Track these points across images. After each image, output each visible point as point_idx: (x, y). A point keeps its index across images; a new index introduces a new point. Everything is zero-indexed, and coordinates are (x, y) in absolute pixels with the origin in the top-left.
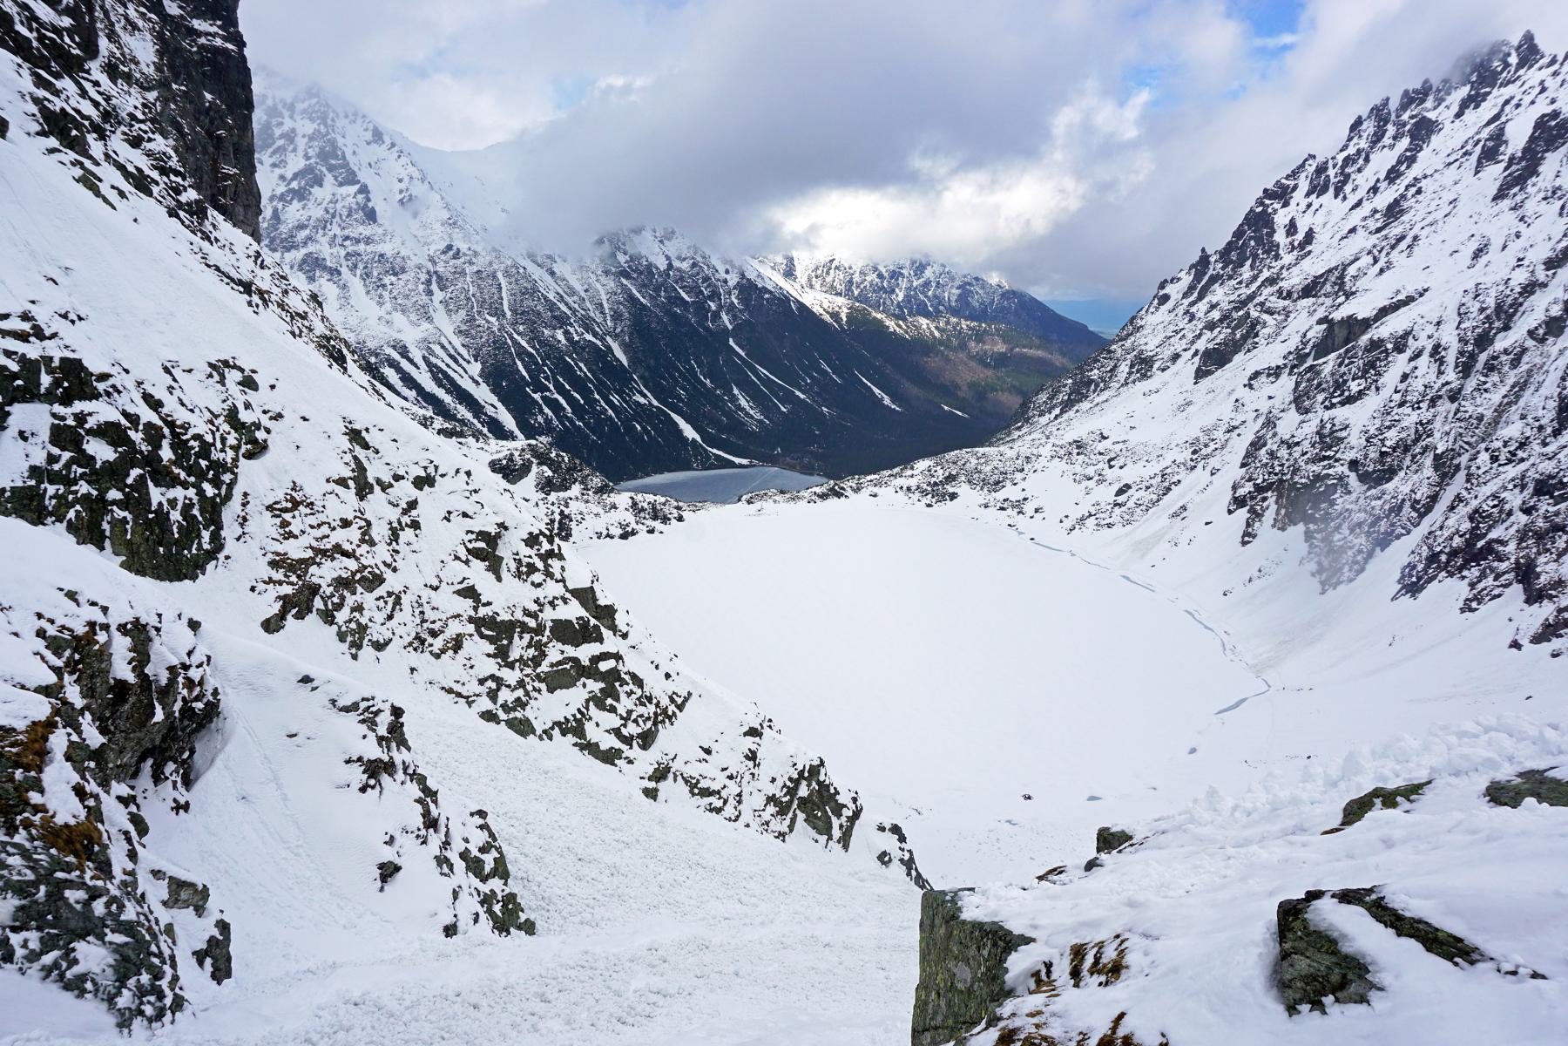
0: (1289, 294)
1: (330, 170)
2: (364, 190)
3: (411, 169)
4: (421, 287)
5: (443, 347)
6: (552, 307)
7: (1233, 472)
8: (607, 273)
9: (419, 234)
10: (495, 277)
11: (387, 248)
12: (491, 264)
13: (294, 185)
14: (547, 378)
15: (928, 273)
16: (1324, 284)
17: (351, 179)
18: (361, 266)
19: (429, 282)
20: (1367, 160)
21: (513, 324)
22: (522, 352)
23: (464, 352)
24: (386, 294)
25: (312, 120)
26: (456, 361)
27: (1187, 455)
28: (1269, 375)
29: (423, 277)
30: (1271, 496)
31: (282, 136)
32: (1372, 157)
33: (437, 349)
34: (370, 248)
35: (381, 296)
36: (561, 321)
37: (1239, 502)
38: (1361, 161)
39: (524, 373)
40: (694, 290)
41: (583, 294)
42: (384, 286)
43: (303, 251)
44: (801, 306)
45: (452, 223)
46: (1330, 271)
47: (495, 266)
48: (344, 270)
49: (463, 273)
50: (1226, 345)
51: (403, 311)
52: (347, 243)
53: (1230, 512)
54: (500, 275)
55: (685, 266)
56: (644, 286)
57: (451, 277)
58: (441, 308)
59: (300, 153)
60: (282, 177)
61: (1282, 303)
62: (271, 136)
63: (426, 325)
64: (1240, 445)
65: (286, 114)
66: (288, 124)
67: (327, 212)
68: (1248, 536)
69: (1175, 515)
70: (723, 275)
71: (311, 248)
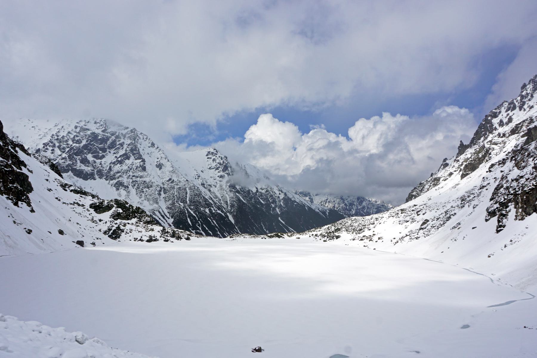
0: (504, 135)
1: (133, 155)
2: (144, 161)
3: (162, 155)
4: (157, 192)
5: (160, 212)
6: (206, 200)
7: (488, 204)
8: (231, 191)
9: (160, 175)
10: (185, 189)
11: (147, 180)
12: (185, 185)
13: (119, 159)
14: (199, 225)
15: (364, 204)
16: (522, 127)
17: (140, 157)
18: (136, 185)
19: (160, 191)
20: (532, 96)
21: (189, 206)
22: (190, 215)
23: (168, 215)
24: (143, 195)
25: (131, 139)
26: (164, 217)
27: (460, 202)
28: (500, 164)
29: (158, 189)
30: (511, 206)
31: (119, 144)
32: (534, 95)
33: (157, 213)
34: (141, 179)
35: (141, 195)
36: (209, 205)
37: (491, 214)
38: (529, 97)
39: (190, 223)
40: (266, 200)
41: (220, 198)
42: (143, 192)
43: (117, 180)
44: (310, 208)
45: (173, 172)
46: (524, 121)
47: (186, 186)
48: (130, 187)
49: (174, 188)
50: (475, 160)
51: (148, 200)
52: (134, 178)
53: (487, 220)
54: (187, 189)
55: (263, 191)
56: (246, 197)
57: (169, 189)
58: (163, 200)
59: (124, 149)
60: (116, 157)
61: (500, 140)
62: (115, 144)
63: (156, 205)
64: (488, 193)
65: (122, 137)
66: (122, 141)
67: (129, 167)
68: (500, 228)
69: (454, 227)
70: (278, 195)
71: (120, 179)
